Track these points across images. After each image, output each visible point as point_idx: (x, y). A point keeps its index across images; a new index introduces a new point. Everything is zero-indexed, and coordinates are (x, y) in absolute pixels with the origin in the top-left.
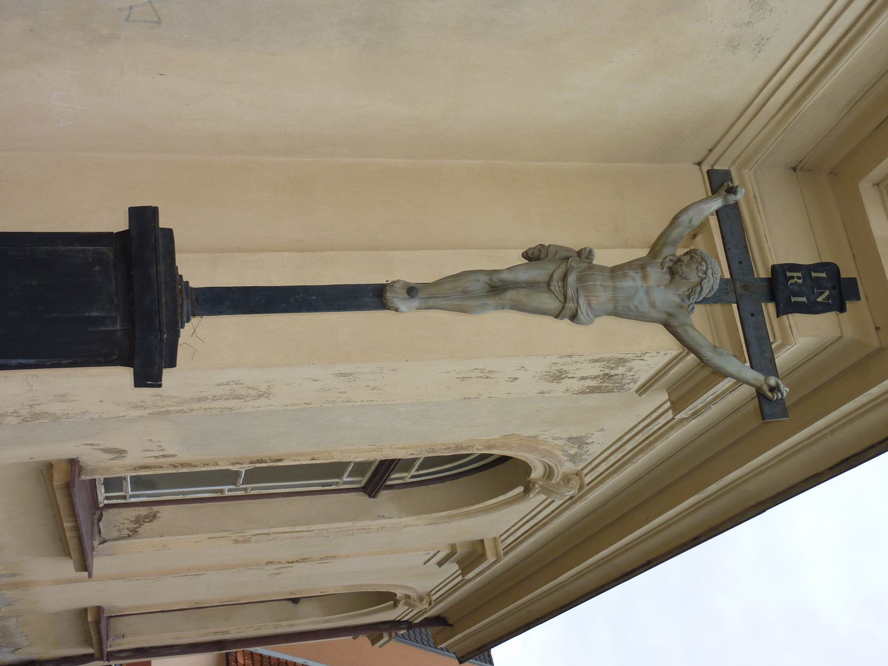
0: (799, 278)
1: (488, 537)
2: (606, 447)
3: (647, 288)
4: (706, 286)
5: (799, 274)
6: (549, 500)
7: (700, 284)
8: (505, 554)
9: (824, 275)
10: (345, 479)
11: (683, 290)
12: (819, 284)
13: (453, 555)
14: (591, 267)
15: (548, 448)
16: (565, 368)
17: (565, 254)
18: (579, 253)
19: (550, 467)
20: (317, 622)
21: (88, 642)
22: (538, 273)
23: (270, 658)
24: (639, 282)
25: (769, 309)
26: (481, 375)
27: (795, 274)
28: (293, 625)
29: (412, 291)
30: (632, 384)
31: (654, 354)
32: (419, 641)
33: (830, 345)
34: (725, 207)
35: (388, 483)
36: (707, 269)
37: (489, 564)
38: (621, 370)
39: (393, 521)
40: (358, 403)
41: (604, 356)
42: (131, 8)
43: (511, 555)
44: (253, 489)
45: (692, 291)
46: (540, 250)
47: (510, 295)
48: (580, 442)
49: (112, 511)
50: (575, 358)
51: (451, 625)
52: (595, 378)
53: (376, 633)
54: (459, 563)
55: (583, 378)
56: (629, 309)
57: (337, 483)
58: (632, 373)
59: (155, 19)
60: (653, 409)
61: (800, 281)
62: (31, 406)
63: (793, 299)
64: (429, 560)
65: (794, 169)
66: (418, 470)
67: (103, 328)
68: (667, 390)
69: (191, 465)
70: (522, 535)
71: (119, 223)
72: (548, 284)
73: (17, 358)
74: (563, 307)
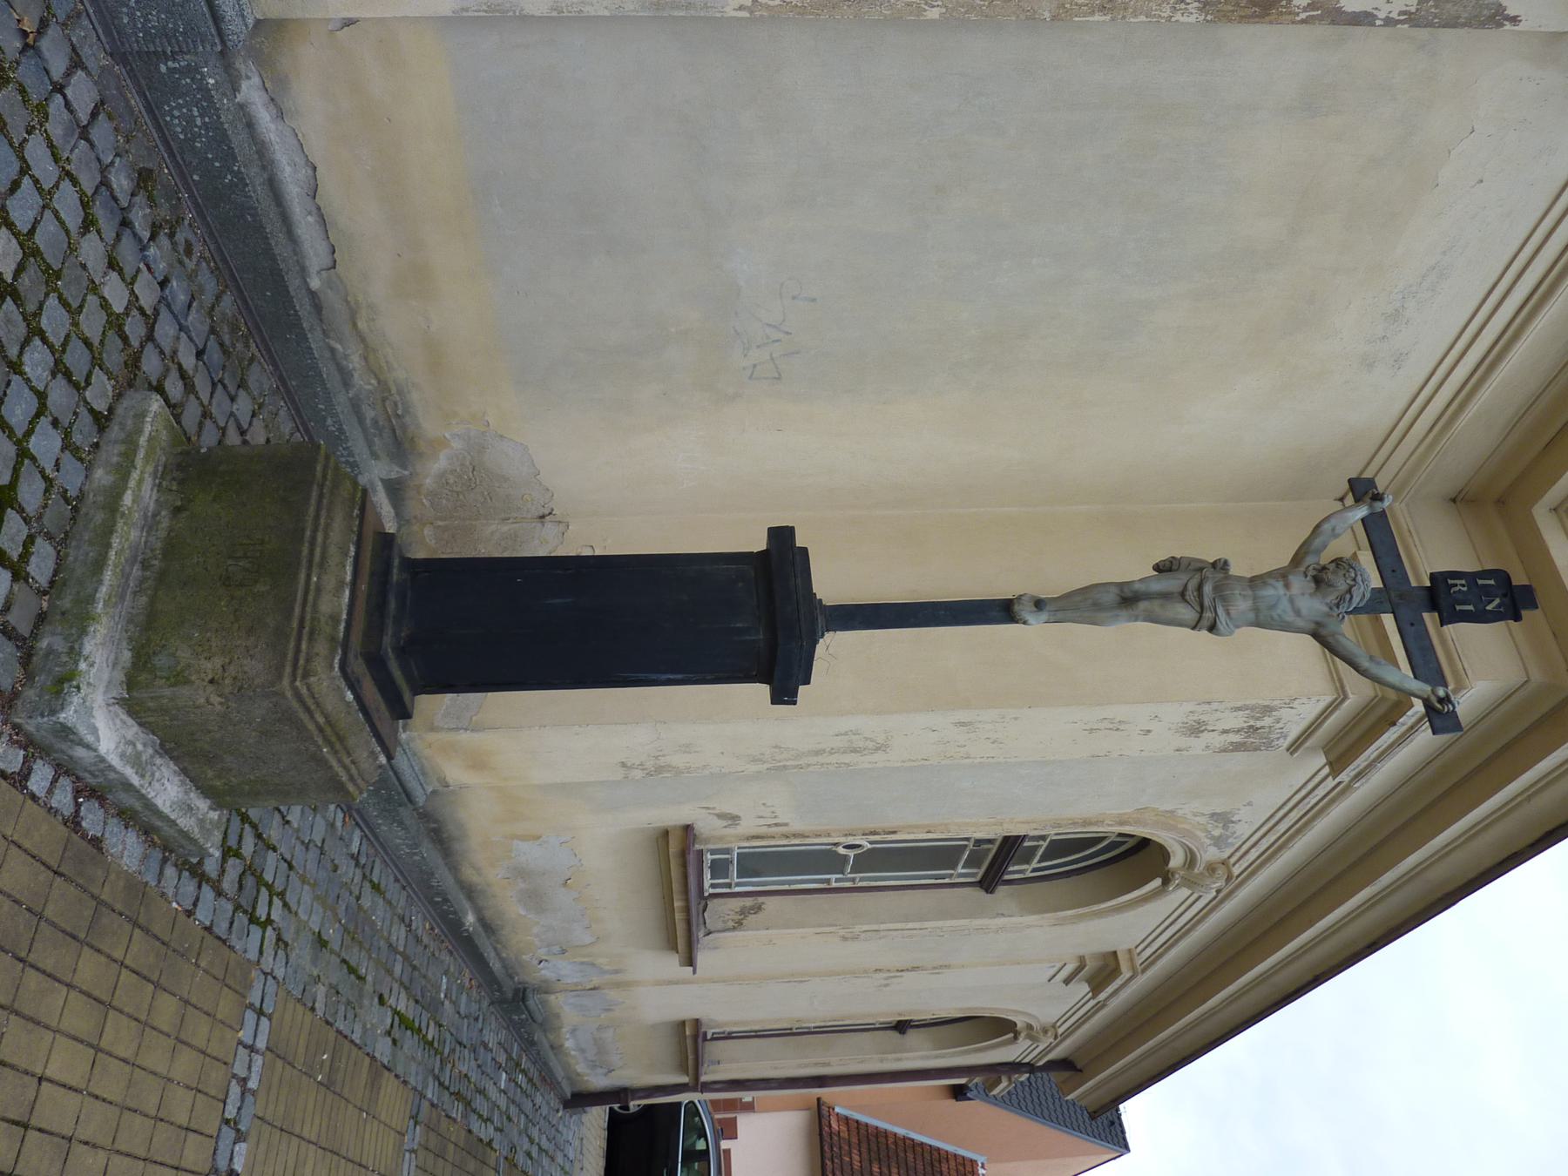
0: (1463, 586)
1: (1121, 949)
2: (1254, 829)
3: (1290, 597)
4: (1356, 600)
5: (1463, 582)
6: (1195, 896)
7: (1349, 591)
8: (1144, 971)
9: (1492, 582)
10: (960, 870)
11: (1332, 598)
12: (1488, 593)
13: (1083, 968)
14: (1228, 577)
15: (1187, 827)
16: (1204, 718)
17: (1199, 565)
18: (1214, 565)
19: (1191, 851)
20: (928, 1058)
21: (683, 1068)
22: (1172, 584)
23: (867, 1125)
24: (1281, 591)
25: (1430, 619)
26: (1111, 726)
27: (1458, 582)
28: (899, 1060)
29: (1039, 604)
30: (1282, 740)
31: (1305, 700)
32: (1039, 1114)
33: (1515, 692)
34: (1372, 514)
35: (1006, 877)
36: (1356, 575)
37: (1124, 980)
38: (1267, 721)
39: (1014, 920)
40: (978, 760)
41: (1248, 703)
42: (755, 366)
43: (1149, 973)
44: (863, 879)
45: (1341, 599)
46: (1171, 562)
47: (1143, 605)
48: (1224, 819)
49: (716, 901)
50: (1215, 706)
51: (1081, 1071)
52: (1239, 731)
53: (994, 1076)
54: (1089, 981)
55: (1225, 732)
56: (1272, 618)
57: (951, 876)
58: (1280, 725)
59: (776, 375)
60: (1308, 777)
61: (1465, 589)
62: (657, 757)
63: (1458, 608)
64: (1054, 976)
65: (1454, 500)
66: (1039, 862)
67: (748, 638)
68: (1323, 748)
69: (803, 836)
70: (1162, 946)
71: (759, 544)
72: (1183, 594)
73: (665, 673)
74: (1201, 617)
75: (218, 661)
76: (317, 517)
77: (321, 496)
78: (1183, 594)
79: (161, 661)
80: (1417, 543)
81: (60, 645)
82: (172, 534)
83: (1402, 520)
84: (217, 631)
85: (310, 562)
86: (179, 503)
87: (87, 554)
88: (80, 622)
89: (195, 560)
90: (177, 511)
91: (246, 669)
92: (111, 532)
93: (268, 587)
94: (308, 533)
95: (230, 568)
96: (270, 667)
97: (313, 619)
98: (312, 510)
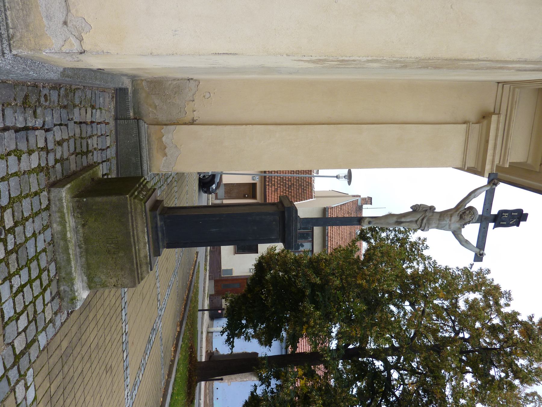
0: (507, 215)
5: (507, 214)
9: (516, 214)
61: (507, 217)
75: (114, 279)
76: (133, 225)
77: (132, 216)
78: (416, 221)
79: (96, 279)
80: (516, 108)
81: (67, 289)
82: (85, 235)
83: (516, 96)
84: (111, 269)
85: (134, 242)
86: (83, 223)
87: (63, 257)
88: (71, 281)
89: (96, 245)
90: (84, 226)
91: (124, 282)
92: (68, 249)
93: (123, 254)
94: (131, 233)
95: (109, 247)
96: (131, 281)
97: (140, 261)
98: (130, 224)
